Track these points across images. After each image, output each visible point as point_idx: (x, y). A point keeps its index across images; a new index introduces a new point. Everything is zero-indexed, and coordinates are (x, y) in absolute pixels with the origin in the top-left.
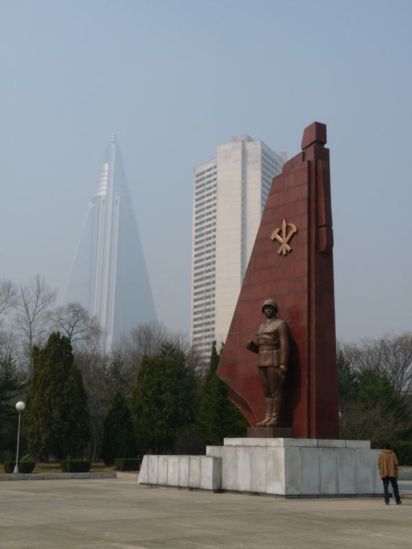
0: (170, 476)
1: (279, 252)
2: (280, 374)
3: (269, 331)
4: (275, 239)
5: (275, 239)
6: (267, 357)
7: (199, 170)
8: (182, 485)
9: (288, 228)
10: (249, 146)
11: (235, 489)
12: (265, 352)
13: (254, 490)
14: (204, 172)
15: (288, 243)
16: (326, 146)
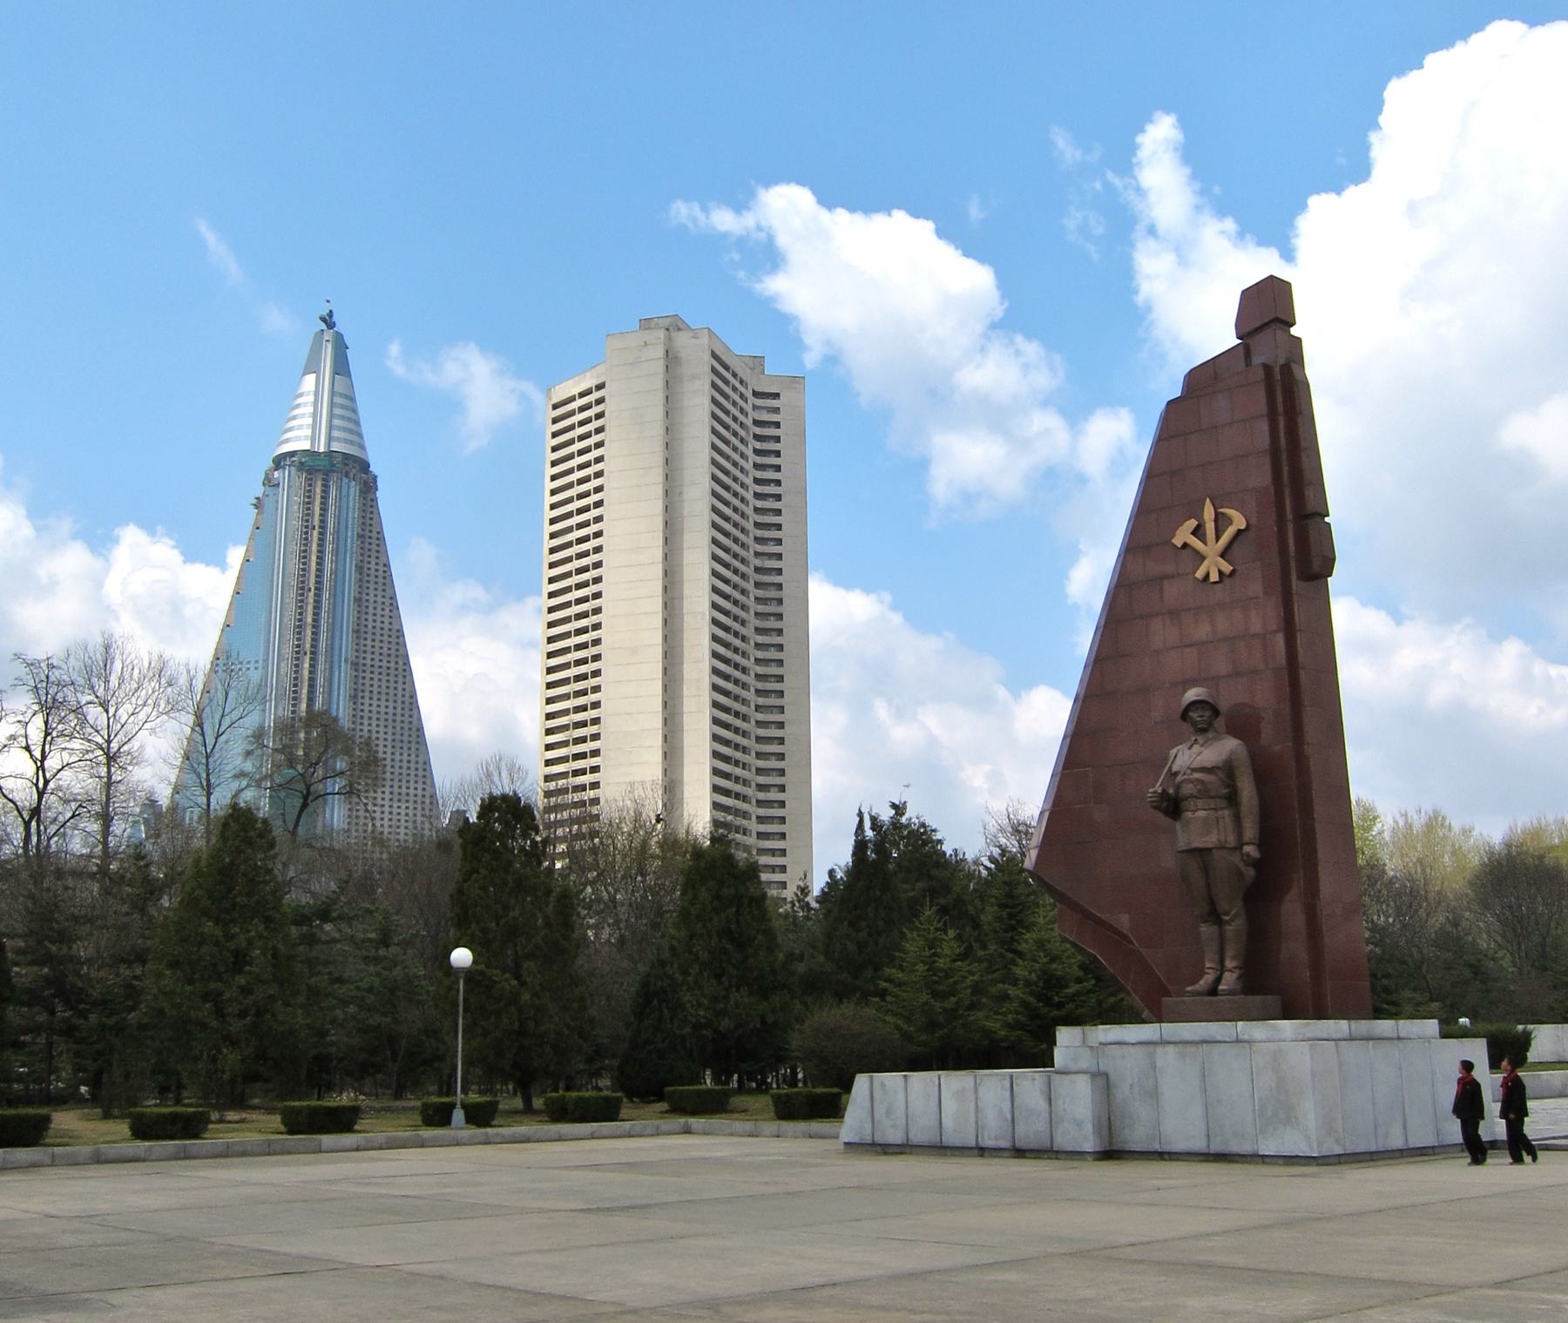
0: (948, 1122)
1: (1200, 574)
2: (1241, 865)
3: (1208, 764)
4: (1185, 545)
5: (1185, 545)
6: (1203, 828)
7: (560, 393)
8: (950, 1139)
9: (1221, 522)
10: (681, 339)
11: (1157, 1147)
12: (1201, 813)
13: (1216, 1147)
14: (572, 399)
15: (1223, 555)
16: (1294, 331)
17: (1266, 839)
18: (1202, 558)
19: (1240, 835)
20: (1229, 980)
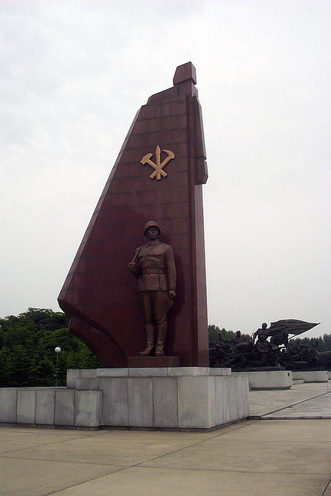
1: (152, 176)
4: (146, 163)
9: (164, 155)
17: (179, 288)
18: (154, 169)
19: (168, 286)
20: (160, 350)
